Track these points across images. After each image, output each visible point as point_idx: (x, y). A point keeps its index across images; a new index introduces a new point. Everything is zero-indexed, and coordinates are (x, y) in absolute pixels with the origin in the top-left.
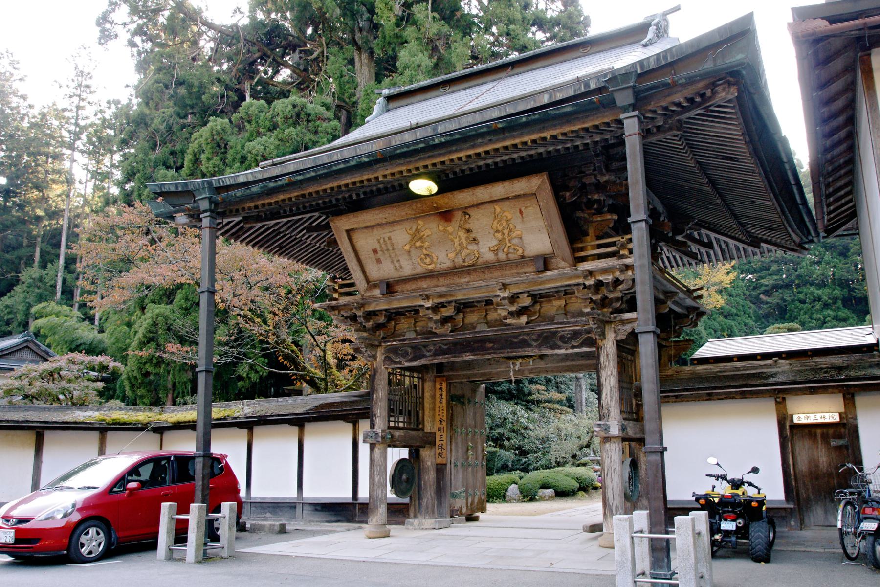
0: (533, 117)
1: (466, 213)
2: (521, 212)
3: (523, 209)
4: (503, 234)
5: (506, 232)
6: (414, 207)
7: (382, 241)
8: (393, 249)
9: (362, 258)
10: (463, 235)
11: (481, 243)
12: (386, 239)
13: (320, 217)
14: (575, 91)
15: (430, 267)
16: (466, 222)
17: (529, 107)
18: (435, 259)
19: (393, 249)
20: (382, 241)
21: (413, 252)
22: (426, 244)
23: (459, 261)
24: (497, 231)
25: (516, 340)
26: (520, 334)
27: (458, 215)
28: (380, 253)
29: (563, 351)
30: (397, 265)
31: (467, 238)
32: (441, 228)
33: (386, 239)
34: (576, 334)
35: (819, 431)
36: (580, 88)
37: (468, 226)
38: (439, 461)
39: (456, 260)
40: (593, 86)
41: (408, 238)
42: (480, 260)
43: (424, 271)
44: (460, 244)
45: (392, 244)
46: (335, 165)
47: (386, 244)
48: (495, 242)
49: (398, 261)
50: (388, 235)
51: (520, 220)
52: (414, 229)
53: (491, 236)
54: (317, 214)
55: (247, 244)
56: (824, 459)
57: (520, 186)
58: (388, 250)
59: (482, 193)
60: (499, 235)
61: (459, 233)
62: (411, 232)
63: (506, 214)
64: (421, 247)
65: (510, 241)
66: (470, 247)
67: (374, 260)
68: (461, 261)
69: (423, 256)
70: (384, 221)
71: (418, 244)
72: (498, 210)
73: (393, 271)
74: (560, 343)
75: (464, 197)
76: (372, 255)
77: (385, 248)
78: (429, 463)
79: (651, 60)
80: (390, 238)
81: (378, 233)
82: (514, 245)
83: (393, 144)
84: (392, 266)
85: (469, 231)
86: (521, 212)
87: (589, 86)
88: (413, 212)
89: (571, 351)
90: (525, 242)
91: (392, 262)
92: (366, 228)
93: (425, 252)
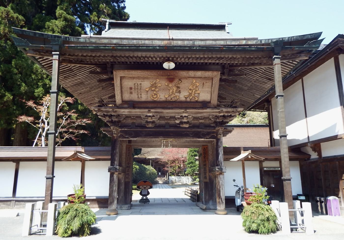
0: (239, 49)
1: (180, 80)
2: (203, 84)
3: (204, 83)
4: (192, 91)
5: (194, 91)
6: (159, 73)
7: (136, 85)
8: (140, 89)
9: (123, 90)
10: (175, 89)
11: (181, 93)
12: (139, 84)
13: (94, 67)
14: (256, 42)
15: (155, 99)
16: (179, 84)
17: (236, 44)
18: (158, 96)
19: (140, 89)
20: (136, 85)
21: (149, 92)
22: (157, 90)
23: (169, 99)
24: (190, 90)
25: (183, 133)
26: (185, 131)
27: (176, 81)
28: (133, 90)
29: (203, 139)
30: (140, 96)
31: (176, 90)
32: (166, 84)
33: (139, 84)
34: (208, 134)
35: (271, 173)
36: (258, 42)
37: (179, 85)
38: (127, 180)
39: (168, 98)
40: (263, 42)
41: (150, 85)
42: (179, 100)
43: (151, 100)
44: (173, 92)
45: (141, 87)
46: (141, 47)
47: (138, 87)
48: (188, 94)
49: (141, 94)
50: (141, 82)
51: (202, 87)
52: (154, 82)
53: (187, 91)
54: (93, 66)
55: (282, 70)
56: (207, 197)
57: (208, 74)
58: (138, 89)
59: (192, 73)
60: (191, 92)
61: (174, 88)
62: (152, 83)
63: (197, 84)
64: (154, 90)
65: (194, 94)
66: (176, 94)
67: (129, 92)
68: (170, 99)
69: (153, 95)
70: (142, 76)
71: (153, 89)
72: (194, 81)
73: (137, 98)
74: (202, 136)
75: (183, 73)
76: (129, 90)
77: (136, 87)
78: (123, 181)
79: (286, 38)
80: (140, 84)
81: (135, 81)
82: (195, 96)
83: (172, 44)
84: (137, 96)
85: (178, 87)
86: (203, 84)
87: (262, 42)
88: (158, 75)
89: (206, 140)
90: (200, 96)
91: (138, 94)
92: (131, 78)
93: (155, 92)
